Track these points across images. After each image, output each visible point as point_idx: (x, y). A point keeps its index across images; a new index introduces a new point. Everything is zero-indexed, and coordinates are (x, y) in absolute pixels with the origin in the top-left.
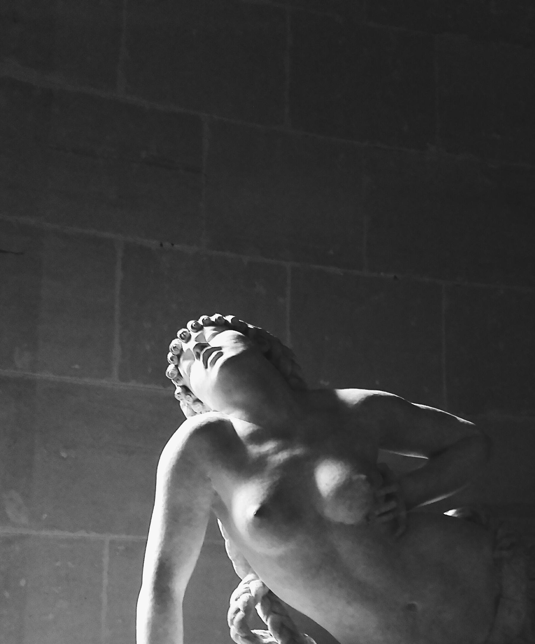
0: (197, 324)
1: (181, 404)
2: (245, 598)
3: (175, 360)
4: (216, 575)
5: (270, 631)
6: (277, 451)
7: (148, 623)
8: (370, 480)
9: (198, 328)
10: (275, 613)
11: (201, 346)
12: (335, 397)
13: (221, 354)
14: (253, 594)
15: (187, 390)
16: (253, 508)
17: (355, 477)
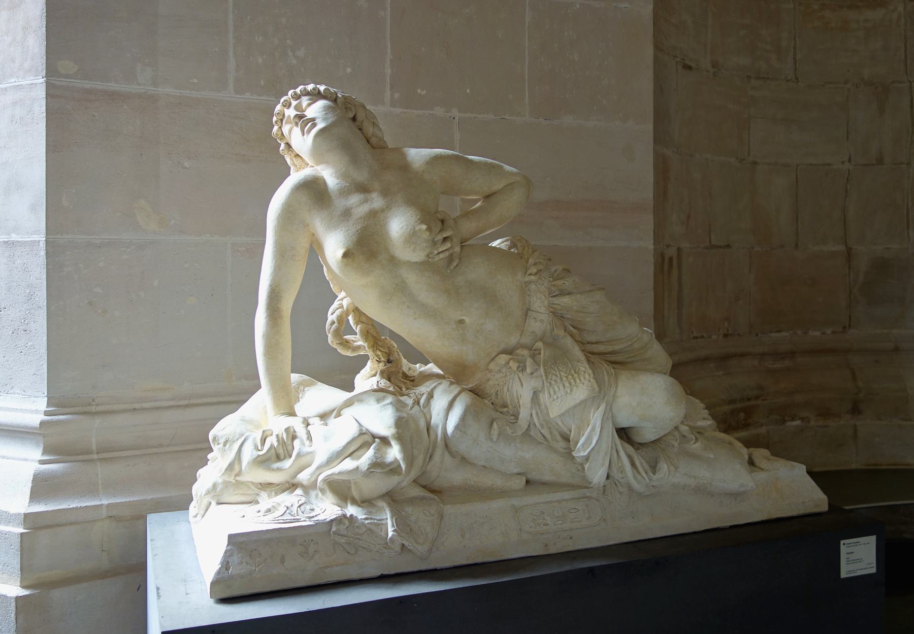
0: (295, 93)
2: (338, 312)
3: (279, 123)
4: (317, 292)
8: (429, 229)
9: (297, 97)
12: (404, 156)
13: (314, 125)
15: (288, 145)
16: (340, 252)
17: (417, 228)
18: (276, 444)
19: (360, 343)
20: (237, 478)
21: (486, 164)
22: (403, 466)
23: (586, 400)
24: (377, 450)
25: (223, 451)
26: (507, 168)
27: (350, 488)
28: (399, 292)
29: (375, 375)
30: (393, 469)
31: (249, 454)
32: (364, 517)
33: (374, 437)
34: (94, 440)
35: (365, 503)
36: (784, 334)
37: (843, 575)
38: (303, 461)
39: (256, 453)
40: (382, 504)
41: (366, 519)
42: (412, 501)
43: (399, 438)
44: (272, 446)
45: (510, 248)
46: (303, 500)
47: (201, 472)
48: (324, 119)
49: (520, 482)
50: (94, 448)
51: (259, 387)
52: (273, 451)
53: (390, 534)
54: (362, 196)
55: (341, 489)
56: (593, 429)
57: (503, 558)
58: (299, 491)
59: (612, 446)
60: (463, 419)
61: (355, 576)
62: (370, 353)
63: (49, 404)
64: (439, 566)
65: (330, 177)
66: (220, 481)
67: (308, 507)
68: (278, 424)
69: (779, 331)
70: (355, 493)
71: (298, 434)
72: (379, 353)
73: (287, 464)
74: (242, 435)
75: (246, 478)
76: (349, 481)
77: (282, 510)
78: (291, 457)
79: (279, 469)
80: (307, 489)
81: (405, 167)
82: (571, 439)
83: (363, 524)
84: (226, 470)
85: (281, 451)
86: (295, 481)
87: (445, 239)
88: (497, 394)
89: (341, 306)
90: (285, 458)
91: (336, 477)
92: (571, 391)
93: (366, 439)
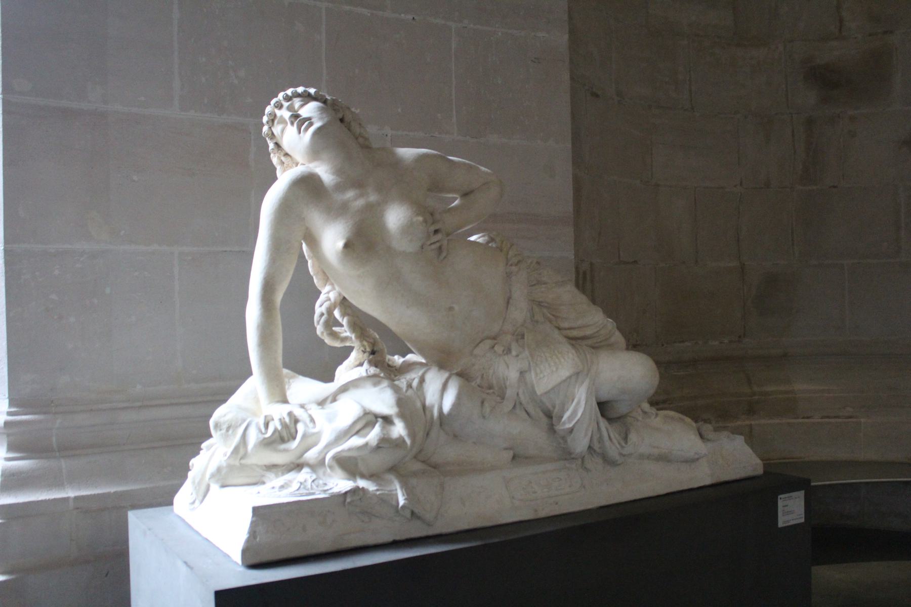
1: (272, 155)
2: (326, 304)
3: (270, 123)
5: (346, 327)
6: (355, 199)
7: (258, 326)
10: (348, 315)
11: (295, 116)
12: (394, 154)
13: (311, 124)
14: (332, 300)
15: (278, 145)
16: (340, 244)
17: (415, 219)
18: (279, 428)
19: (348, 334)
20: (243, 462)
21: (465, 164)
22: (408, 441)
23: (570, 377)
24: (383, 428)
25: (226, 437)
26: (483, 169)
27: (356, 465)
28: (391, 282)
29: (361, 365)
30: (399, 443)
31: (253, 438)
32: (375, 488)
33: (376, 416)
34: (54, 439)
35: (371, 476)
36: (687, 344)
37: (781, 524)
38: (310, 441)
39: (261, 437)
40: (391, 477)
41: (377, 490)
42: (415, 474)
43: (402, 415)
44: (276, 430)
45: (488, 242)
46: (314, 477)
47: (194, 462)
48: (321, 119)
49: (508, 455)
50: (55, 446)
51: (250, 374)
52: (277, 434)
53: (402, 501)
54: (357, 191)
55: (348, 465)
56: (578, 403)
57: (499, 523)
58: (306, 470)
59: (585, 419)
60: (459, 397)
61: (371, 540)
62: (356, 344)
63: (12, 403)
64: (445, 530)
65: (324, 172)
66: (224, 464)
67: (321, 482)
68: (279, 412)
69: (683, 342)
70: (362, 468)
71: (300, 418)
72: (365, 343)
73: (294, 445)
74: (244, 421)
75: (252, 460)
76: (355, 458)
77: (295, 486)
78: (294, 438)
79: (286, 450)
80: (317, 466)
81: (396, 164)
82: (554, 415)
83: (375, 495)
84: (232, 453)
85: (285, 434)
86: (301, 461)
87: (436, 232)
88: (482, 377)
89: (329, 299)
90: (289, 440)
91: (345, 454)
92: (557, 369)
93: (369, 419)
